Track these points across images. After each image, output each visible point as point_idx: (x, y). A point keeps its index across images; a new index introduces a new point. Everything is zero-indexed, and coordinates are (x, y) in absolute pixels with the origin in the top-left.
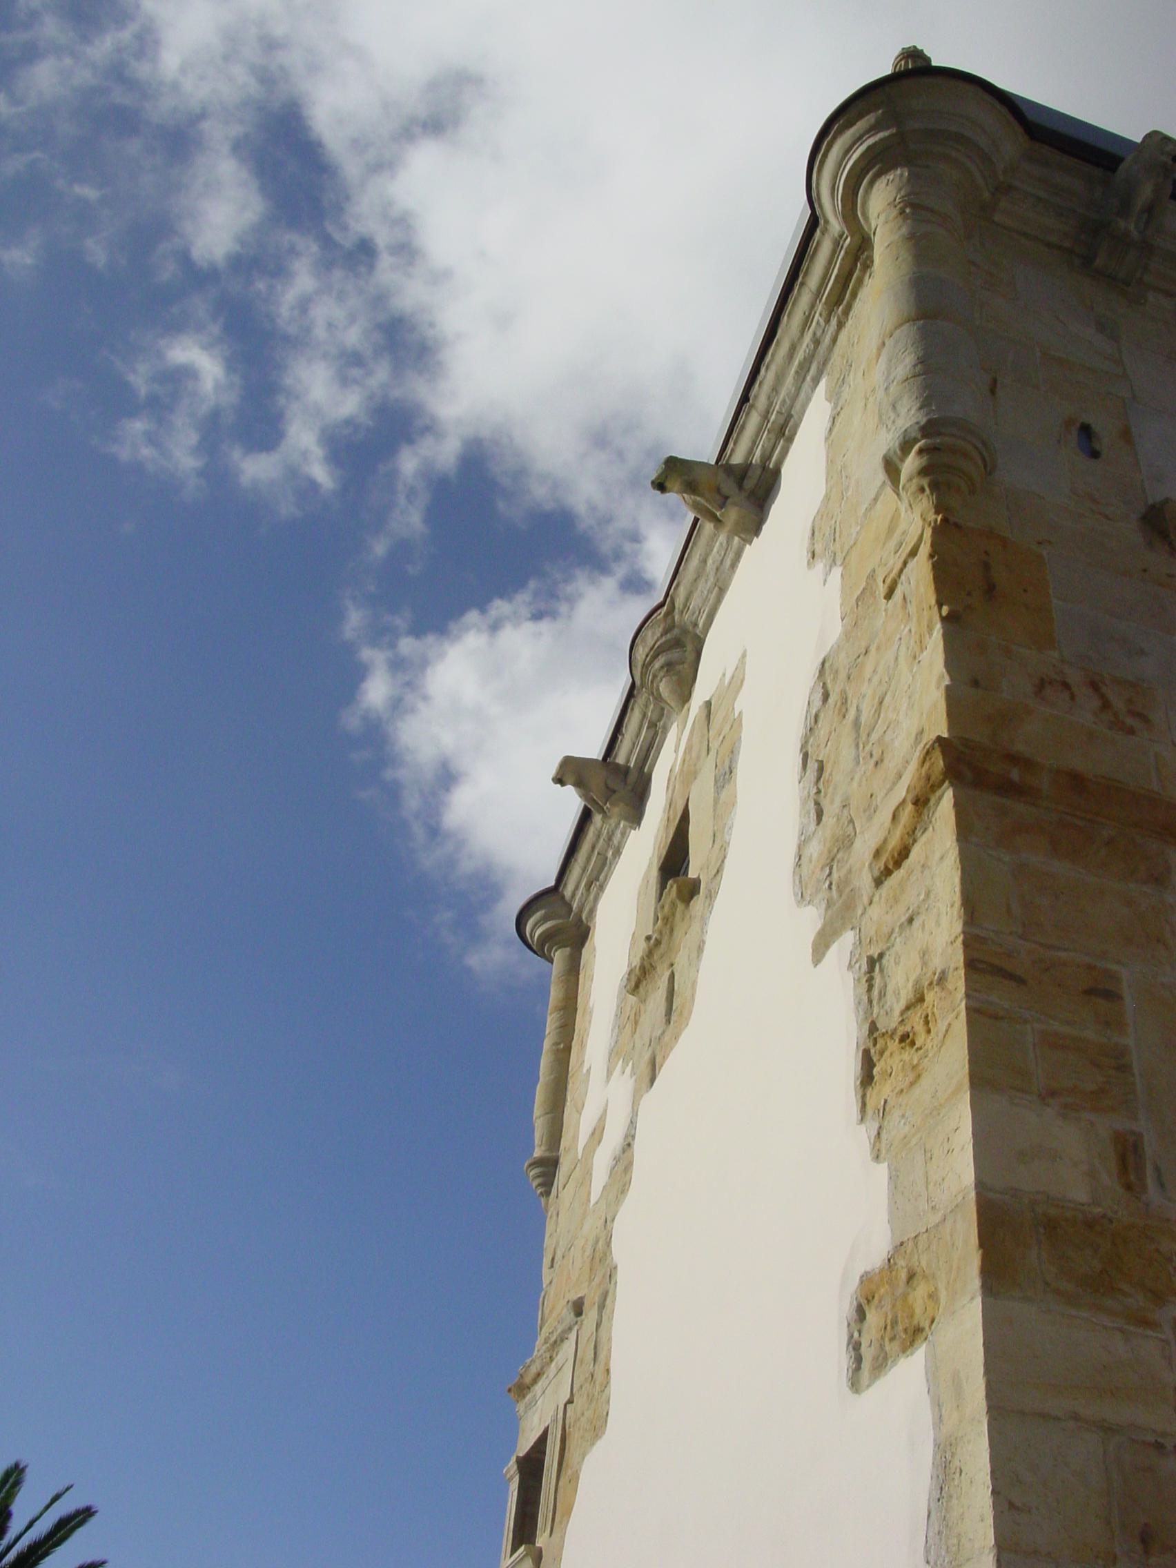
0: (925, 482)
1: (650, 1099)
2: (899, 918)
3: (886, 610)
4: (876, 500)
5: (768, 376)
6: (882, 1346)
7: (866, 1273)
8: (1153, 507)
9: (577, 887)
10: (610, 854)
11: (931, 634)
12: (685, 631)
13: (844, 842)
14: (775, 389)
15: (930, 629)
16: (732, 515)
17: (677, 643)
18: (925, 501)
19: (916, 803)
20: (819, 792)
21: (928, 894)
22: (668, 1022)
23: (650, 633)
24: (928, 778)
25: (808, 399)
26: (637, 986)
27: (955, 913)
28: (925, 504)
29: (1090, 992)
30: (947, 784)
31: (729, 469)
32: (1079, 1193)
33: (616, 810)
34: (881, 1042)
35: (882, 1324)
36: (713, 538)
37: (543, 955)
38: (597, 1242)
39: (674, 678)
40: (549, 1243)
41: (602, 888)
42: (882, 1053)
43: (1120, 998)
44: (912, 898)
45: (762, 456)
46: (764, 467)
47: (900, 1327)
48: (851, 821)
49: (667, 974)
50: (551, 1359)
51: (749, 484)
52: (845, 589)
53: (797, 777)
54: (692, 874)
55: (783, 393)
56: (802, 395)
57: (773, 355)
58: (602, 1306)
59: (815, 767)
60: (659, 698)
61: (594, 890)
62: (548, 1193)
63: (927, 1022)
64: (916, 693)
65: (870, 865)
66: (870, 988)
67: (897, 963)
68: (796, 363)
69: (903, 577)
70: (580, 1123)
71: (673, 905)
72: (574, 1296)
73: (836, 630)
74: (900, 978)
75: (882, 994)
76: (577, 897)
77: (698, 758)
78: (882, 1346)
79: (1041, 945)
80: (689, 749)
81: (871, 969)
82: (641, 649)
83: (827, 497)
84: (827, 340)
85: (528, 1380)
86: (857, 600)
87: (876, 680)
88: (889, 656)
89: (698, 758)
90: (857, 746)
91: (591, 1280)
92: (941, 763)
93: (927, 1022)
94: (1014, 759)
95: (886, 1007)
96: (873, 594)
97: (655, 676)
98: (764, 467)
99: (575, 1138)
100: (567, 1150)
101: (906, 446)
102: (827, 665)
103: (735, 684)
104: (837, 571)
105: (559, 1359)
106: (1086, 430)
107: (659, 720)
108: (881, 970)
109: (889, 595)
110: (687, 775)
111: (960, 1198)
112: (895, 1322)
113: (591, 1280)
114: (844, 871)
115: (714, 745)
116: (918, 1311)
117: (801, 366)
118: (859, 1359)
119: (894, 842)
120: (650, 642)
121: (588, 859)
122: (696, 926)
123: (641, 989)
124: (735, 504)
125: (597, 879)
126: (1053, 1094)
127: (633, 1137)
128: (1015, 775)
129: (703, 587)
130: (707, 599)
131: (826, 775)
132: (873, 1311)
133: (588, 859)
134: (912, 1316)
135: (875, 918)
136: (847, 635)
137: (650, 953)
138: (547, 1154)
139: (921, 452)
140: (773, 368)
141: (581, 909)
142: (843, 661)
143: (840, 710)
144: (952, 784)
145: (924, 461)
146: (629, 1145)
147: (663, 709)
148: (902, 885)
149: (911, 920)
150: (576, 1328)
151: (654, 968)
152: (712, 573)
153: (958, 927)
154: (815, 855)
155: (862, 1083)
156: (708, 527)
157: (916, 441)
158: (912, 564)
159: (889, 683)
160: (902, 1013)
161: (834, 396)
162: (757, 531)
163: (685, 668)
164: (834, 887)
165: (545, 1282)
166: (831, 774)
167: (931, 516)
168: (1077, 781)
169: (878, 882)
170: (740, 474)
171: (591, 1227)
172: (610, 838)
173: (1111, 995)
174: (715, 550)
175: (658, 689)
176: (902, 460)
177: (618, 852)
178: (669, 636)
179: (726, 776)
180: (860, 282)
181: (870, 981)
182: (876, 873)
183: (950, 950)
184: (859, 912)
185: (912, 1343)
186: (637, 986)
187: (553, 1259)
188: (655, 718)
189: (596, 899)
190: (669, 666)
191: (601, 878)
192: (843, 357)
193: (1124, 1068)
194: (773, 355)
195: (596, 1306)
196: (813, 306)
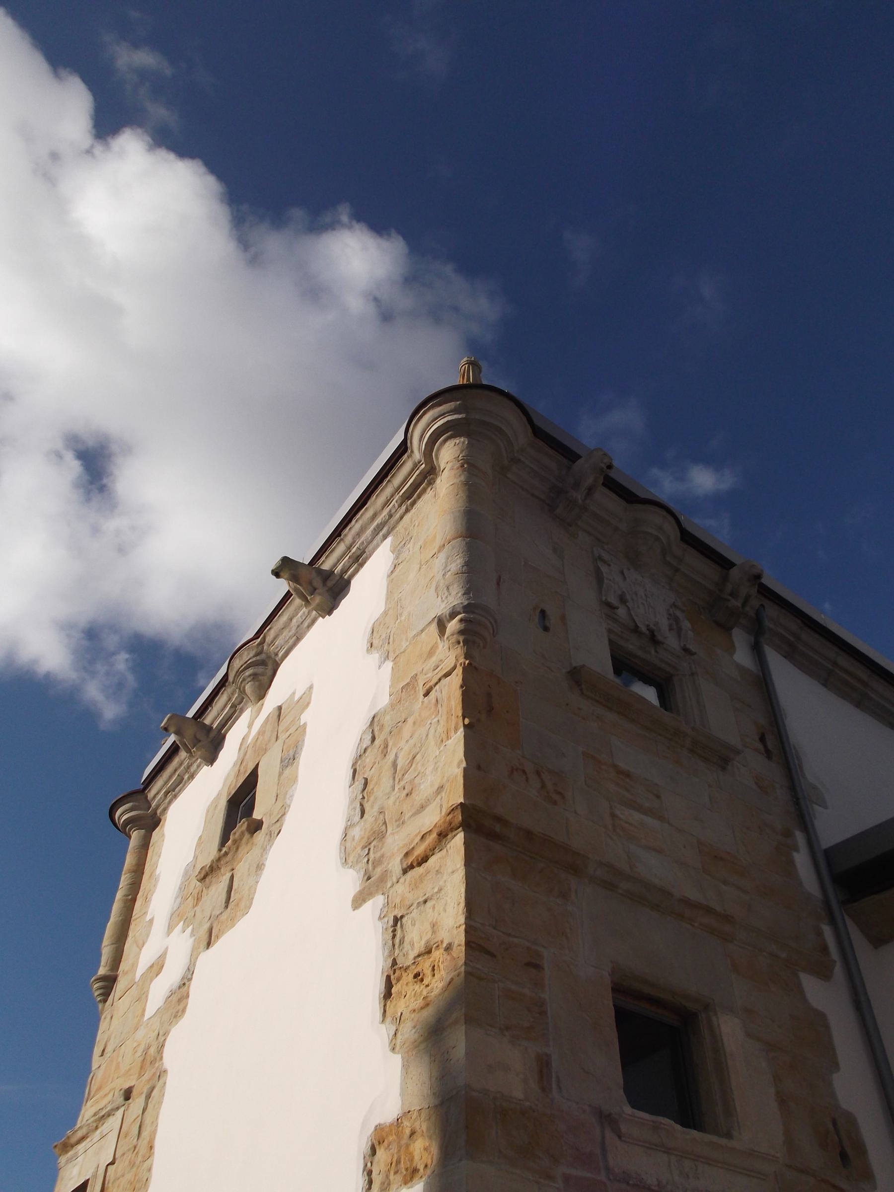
0: (461, 639)
1: (206, 958)
2: (418, 898)
3: (423, 702)
4: (422, 631)
5: (355, 526)
6: (387, 1176)
7: (380, 1125)
8: (575, 668)
9: (158, 793)
10: (186, 777)
11: (456, 733)
12: (269, 657)
13: (378, 836)
14: (359, 535)
15: (456, 730)
16: (317, 599)
17: (263, 663)
18: (459, 649)
19: (440, 835)
20: (364, 798)
21: (440, 890)
22: (227, 907)
23: (246, 653)
24: (450, 823)
25: (378, 546)
26: (205, 877)
27: (461, 912)
28: (459, 651)
29: (529, 964)
30: (461, 829)
31: (320, 571)
32: (518, 1094)
33: (199, 753)
34: (398, 973)
35: (389, 1161)
36: (299, 608)
37: (125, 833)
38: (149, 1048)
39: (257, 683)
40: (101, 1037)
41: (175, 797)
42: (398, 980)
43: (543, 969)
44: (429, 888)
45: (342, 570)
46: (341, 576)
47: (402, 1165)
48: (385, 823)
49: (229, 875)
50: (97, 1128)
51: (330, 583)
52: (394, 679)
53: (348, 784)
54: (257, 815)
55: (363, 538)
56: (375, 542)
57: (362, 515)
58: (148, 1097)
59: (362, 781)
60: (243, 692)
61: (169, 797)
62: (105, 1001)
63: (433, 970)
64: (441, 764)
65: (401, 860)
66: (394, 937)
67: (414, 925)
68: (375, 524)
69: (437, 687)
70: (141, 956)
71: (242, 834)
72: (126, 1086)
73: (384, 700)
74: (416, 936)
75: (402, 942)
76: (157, 800)
77: (269, 741)
78: (387, 1176)
79: (504, 933)
80: (261, 732)
81: (395, 924)
82: (238, 661)
83: (385, 613)
84: (397, 516)
85: (73, 1140)
86: (403, 688)
87: (412, 742)
88: (422, 731)
89: (269, 741)
90: (394, 778)
91: (140, 1076)
92: (460, 818)
93: (433, 970)
94: (499, 819)
95: (404, 951)
96: (414, 688)
97: (244, 680)
98: (341, 576)
99: (134, 966)
100: (125, 973)
101: (453, 615)
102: (376, 720)
103: (304, 702)
104: (389, 665)
105: (104, 1128)
106: (543, 612)
107: (239, 704)
108: (402, 926)
109: (426, 694)
110: (260, 747)
111: (454, 1092)
112: (398, 1162)
113: (140, 1076)
114: (378, 855)
115: (282, 737)
116: (417, 1158)
117: (378, 526)
118: (370, 1182)
119: (419, 851)
120: (245, 658)
121: (170, 777)
122: (256, 851)
123: (207, 880)
124: (320, 594)
125: (174, 790)
126: (507, 1028)
127: (190, 980)
128: (498, 828)
129: (286, 634)
130: (287, 641)
131: (369, 788)
132: (382, 1149)
133: (170, 777)
134: (412, 1160)
135: (400, 891)
136: (392, 706)
137: (219, 859)
138: (109, 973)
139: (461, 620)
140: (360, 522)
141: (158, 806)
142: (388, 721)
143: (382, 752)
144: (464, 830)
145: (462, 626)
146: (184, 984)
147: (243, 698)
148: (421, 878)
149: (425, 902)
150: (122, 1109)
151: (219, 868)
152: (294, 628)
153: (462, 919)
154: (357, 838)
155: (384, 997)
156: (297, 601)
157: (459, 613)
158: (445, 681)
159: (421, 748)
160: (415, 958)
161: (397, 550)
162: (330, 613)
163: (265, 679)
164: (370, 862)
165: (94, 1066)
166: (373, 789)
167: (462, 660)
168: (529, 834)
169: (405, 872)
170: (327, 576)
171: (143, 1036)
172: (189, 767)
173: (538, 967)
174: (300, 614)
175: (244, 687)
176: (449, 622)
177: (192, 777)
178: (258, 658)
179: (290, 760)
180: (424, 490)
181: (394, 931)
182: (405, 866)
183: (455, 932)
184: (389, 885)
185: (411, 1179)
186: (205, 877)
187: (104, 1051)
188: (236, 702)
189: (170, 803)
190: (255, 676)
191: (177, 790)
192: (406, 529)
193: (543, 1013)
194: (362, 515)
195: (144, 1096)
196: (392, 496)
